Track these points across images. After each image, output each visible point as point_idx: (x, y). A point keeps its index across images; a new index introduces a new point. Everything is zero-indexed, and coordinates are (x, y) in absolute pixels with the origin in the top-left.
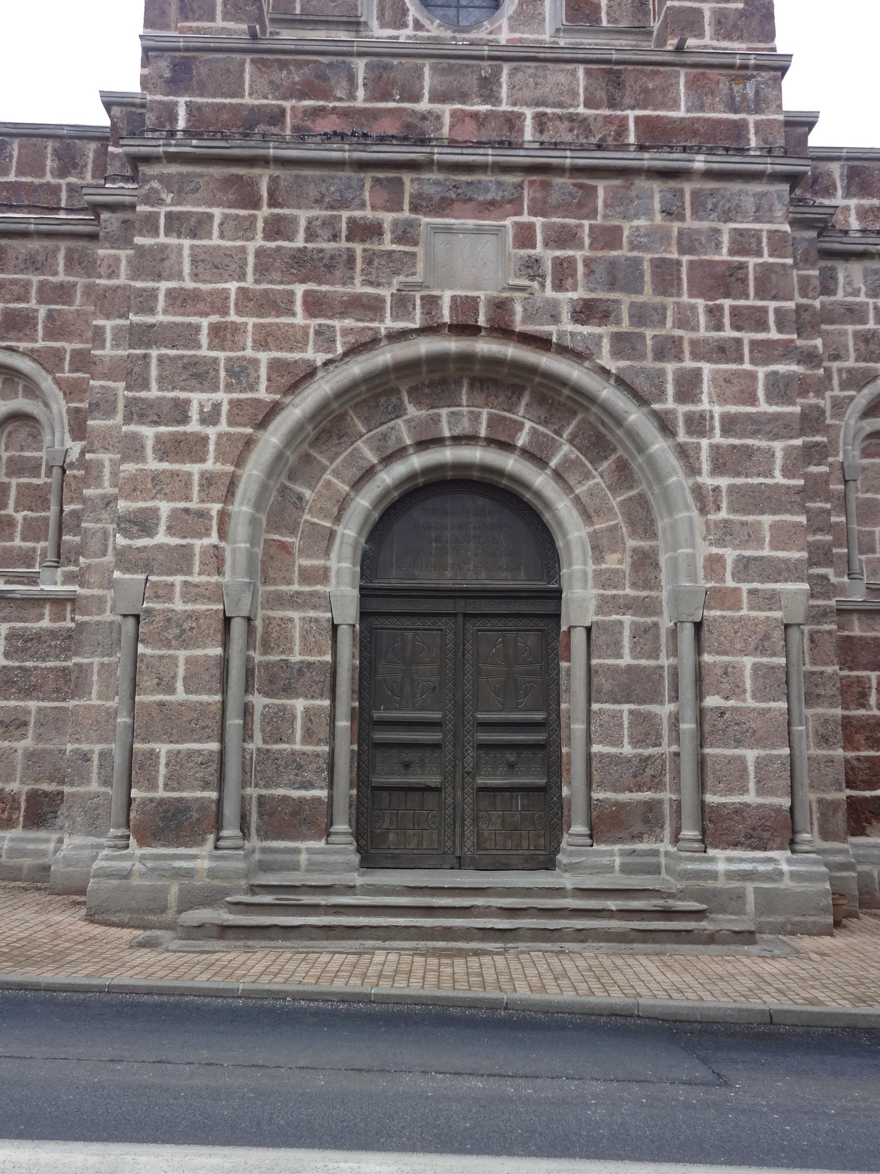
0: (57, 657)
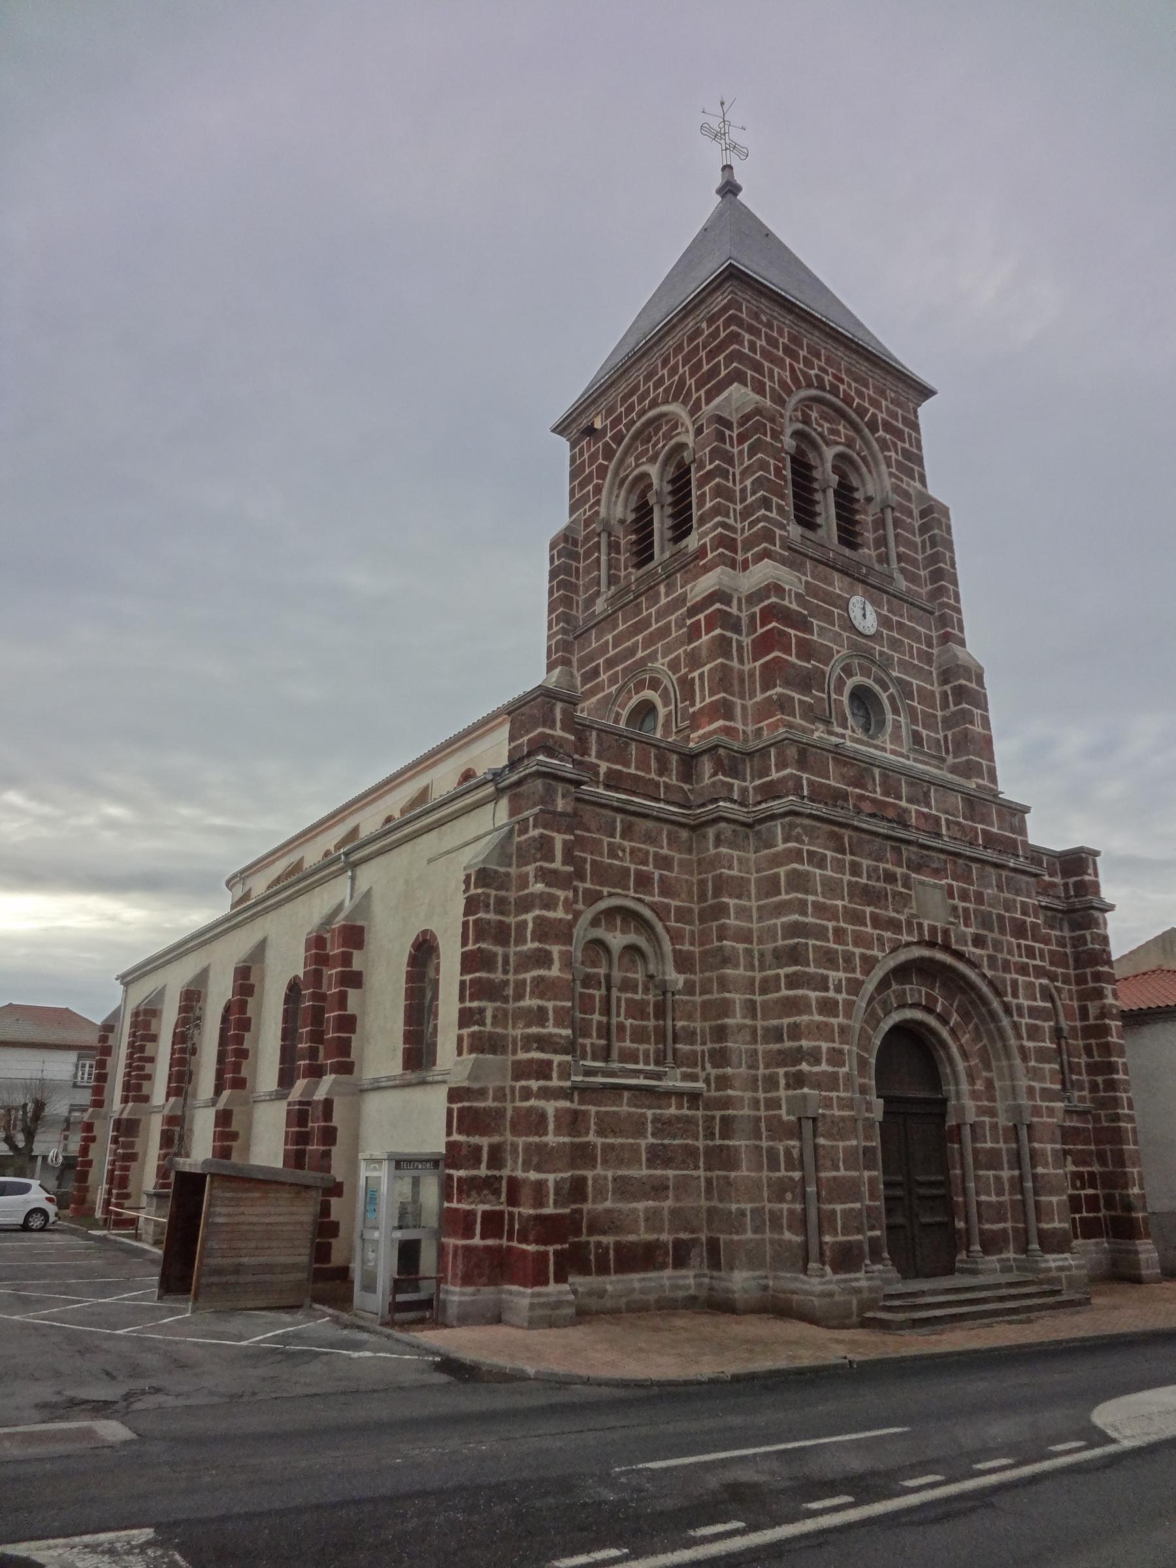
0: (682, 1137)
